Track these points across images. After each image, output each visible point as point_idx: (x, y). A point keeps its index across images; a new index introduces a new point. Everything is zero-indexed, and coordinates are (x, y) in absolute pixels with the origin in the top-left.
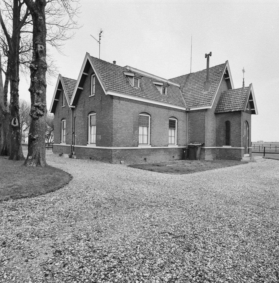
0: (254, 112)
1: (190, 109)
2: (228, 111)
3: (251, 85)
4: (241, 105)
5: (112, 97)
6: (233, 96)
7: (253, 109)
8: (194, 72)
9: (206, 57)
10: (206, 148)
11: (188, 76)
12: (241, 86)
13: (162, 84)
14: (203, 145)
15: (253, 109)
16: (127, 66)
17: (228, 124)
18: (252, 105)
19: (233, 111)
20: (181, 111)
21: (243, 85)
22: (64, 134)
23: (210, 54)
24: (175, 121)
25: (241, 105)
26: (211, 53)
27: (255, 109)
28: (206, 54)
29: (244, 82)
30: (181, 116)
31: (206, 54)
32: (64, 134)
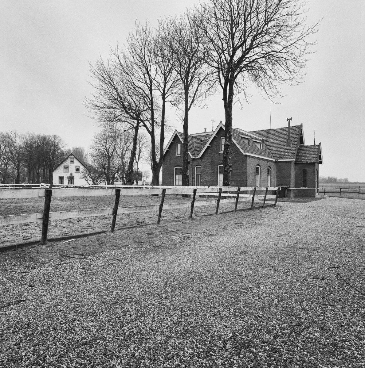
0: (321, 163)
1: (278, 160)
2: (305, 162)
3: (320, 143)
4: (315, 158)
5: (246, 156)
6: (308, 151)
7: (320, 161)
8: (274, 128)
9: (287, 121)
10: (291, 189)
11: (269, 131)
12: (313, 144)
13: (249, 138)
14: (290, 187)
15: (320, 161)
16: (238, 129)
17: (304, 172)
18: (320, 158)
19: (309, 162)
20: (273, 161)
21: (315, 143)
22: (257, 181)
23: (291, 119)
24: (258, 168)
25: (315, 158)
26: (292, 118)
27: (322, 161)
28: (287, 118)
29: (315, 141)
30: (272, 165)
31: (287, 118)
32: (257, 181)
